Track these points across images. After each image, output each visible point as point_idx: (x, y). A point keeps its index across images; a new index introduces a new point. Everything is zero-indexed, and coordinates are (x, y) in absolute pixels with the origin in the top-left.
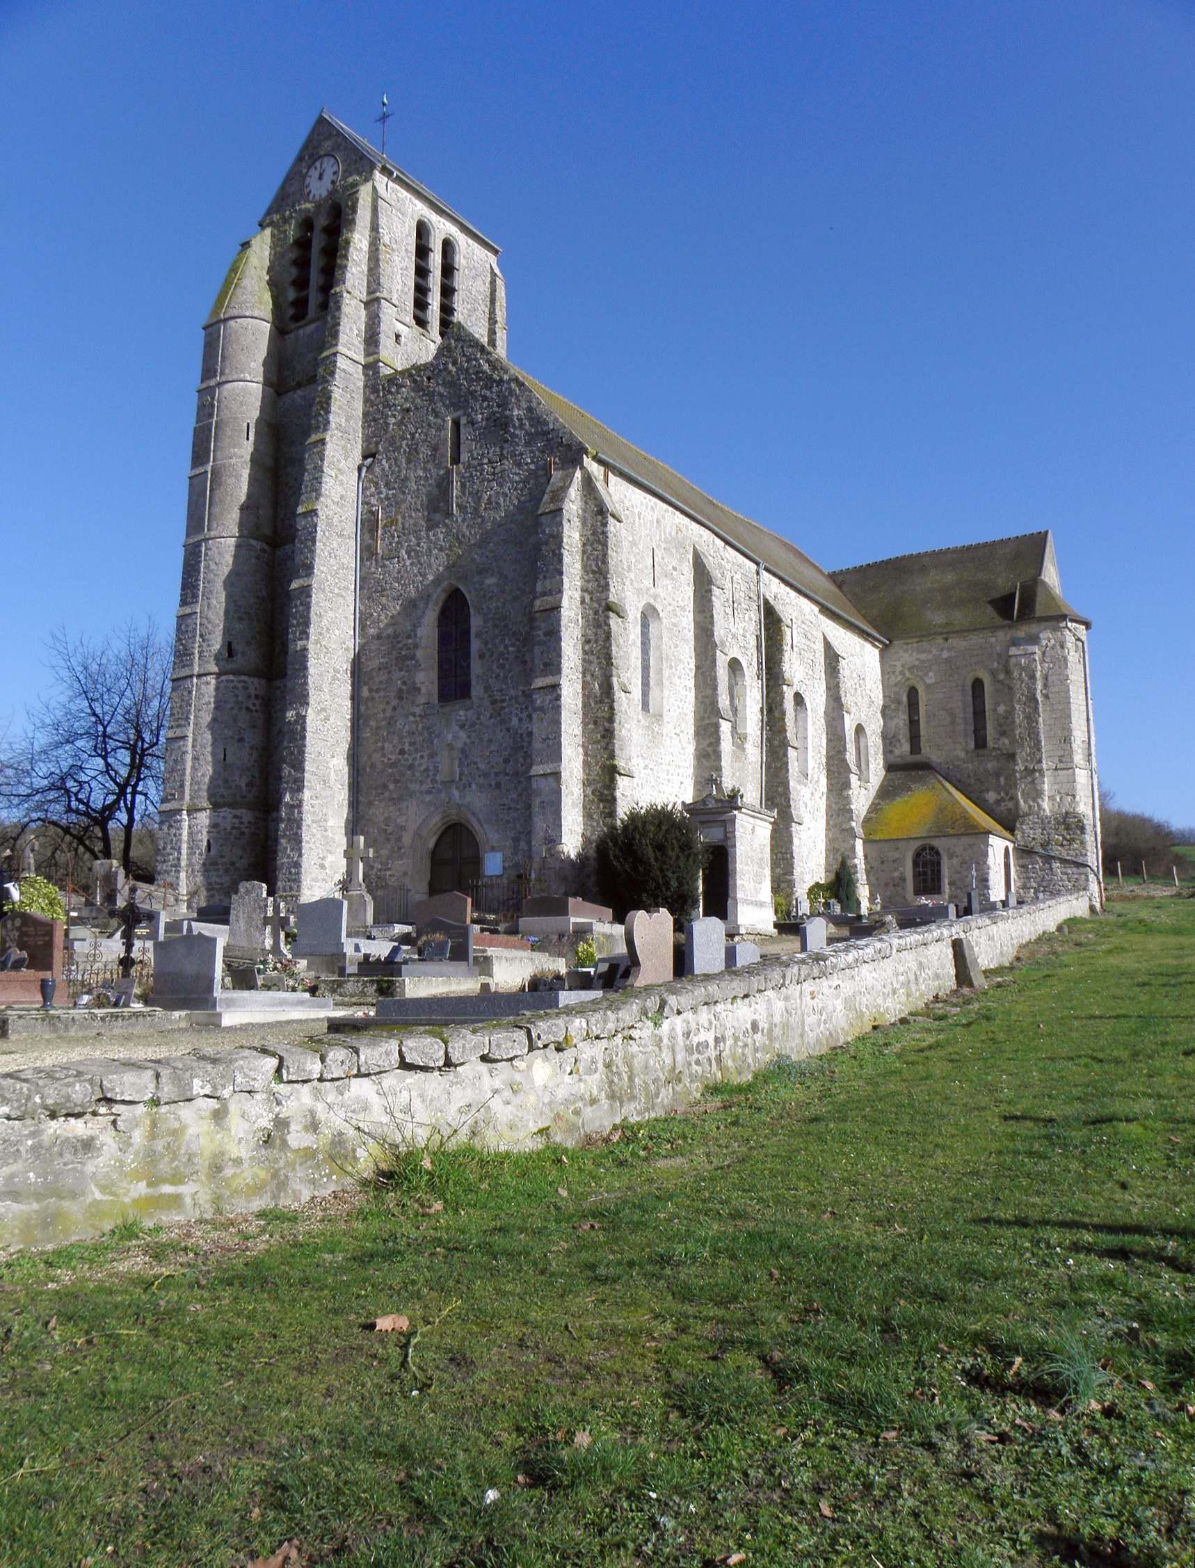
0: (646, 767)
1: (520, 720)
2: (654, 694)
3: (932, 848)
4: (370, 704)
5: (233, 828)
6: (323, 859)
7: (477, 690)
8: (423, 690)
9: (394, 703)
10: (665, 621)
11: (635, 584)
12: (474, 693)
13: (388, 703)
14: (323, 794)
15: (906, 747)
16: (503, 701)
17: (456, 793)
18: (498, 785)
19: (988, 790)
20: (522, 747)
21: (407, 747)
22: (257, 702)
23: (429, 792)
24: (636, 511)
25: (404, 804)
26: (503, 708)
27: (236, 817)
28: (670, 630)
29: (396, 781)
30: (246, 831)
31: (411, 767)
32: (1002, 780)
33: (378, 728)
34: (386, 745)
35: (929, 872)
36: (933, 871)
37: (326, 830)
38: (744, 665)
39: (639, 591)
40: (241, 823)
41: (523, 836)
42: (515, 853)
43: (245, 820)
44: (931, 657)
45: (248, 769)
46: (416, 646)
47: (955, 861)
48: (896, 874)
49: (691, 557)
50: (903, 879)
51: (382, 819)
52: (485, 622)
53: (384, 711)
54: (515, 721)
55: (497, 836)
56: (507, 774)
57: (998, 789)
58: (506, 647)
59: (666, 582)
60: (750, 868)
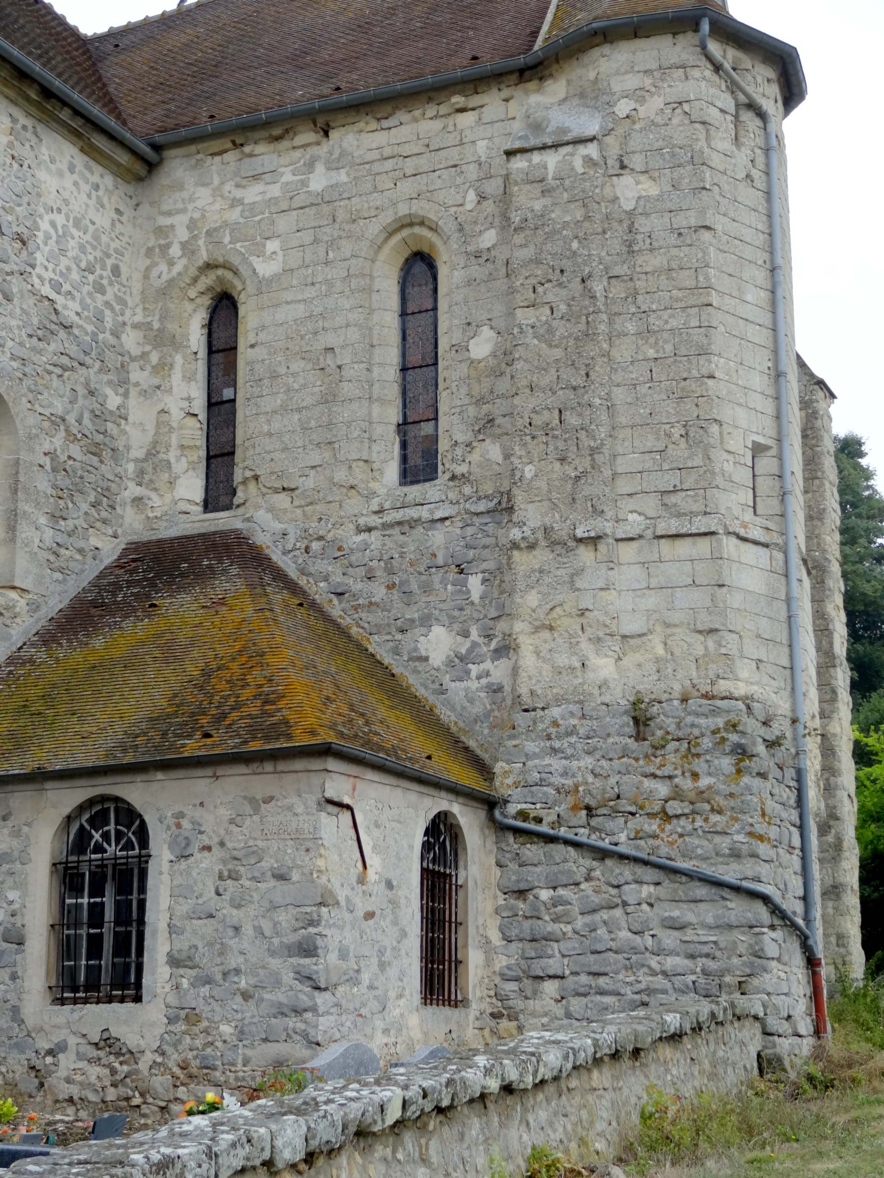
3: (130, 816)
15: (192, 487)
19: (426, 621)
32: (475, 584)
35: (109, 914)
36: (122, 909)
44: (275, 191)
47: (206, 865)
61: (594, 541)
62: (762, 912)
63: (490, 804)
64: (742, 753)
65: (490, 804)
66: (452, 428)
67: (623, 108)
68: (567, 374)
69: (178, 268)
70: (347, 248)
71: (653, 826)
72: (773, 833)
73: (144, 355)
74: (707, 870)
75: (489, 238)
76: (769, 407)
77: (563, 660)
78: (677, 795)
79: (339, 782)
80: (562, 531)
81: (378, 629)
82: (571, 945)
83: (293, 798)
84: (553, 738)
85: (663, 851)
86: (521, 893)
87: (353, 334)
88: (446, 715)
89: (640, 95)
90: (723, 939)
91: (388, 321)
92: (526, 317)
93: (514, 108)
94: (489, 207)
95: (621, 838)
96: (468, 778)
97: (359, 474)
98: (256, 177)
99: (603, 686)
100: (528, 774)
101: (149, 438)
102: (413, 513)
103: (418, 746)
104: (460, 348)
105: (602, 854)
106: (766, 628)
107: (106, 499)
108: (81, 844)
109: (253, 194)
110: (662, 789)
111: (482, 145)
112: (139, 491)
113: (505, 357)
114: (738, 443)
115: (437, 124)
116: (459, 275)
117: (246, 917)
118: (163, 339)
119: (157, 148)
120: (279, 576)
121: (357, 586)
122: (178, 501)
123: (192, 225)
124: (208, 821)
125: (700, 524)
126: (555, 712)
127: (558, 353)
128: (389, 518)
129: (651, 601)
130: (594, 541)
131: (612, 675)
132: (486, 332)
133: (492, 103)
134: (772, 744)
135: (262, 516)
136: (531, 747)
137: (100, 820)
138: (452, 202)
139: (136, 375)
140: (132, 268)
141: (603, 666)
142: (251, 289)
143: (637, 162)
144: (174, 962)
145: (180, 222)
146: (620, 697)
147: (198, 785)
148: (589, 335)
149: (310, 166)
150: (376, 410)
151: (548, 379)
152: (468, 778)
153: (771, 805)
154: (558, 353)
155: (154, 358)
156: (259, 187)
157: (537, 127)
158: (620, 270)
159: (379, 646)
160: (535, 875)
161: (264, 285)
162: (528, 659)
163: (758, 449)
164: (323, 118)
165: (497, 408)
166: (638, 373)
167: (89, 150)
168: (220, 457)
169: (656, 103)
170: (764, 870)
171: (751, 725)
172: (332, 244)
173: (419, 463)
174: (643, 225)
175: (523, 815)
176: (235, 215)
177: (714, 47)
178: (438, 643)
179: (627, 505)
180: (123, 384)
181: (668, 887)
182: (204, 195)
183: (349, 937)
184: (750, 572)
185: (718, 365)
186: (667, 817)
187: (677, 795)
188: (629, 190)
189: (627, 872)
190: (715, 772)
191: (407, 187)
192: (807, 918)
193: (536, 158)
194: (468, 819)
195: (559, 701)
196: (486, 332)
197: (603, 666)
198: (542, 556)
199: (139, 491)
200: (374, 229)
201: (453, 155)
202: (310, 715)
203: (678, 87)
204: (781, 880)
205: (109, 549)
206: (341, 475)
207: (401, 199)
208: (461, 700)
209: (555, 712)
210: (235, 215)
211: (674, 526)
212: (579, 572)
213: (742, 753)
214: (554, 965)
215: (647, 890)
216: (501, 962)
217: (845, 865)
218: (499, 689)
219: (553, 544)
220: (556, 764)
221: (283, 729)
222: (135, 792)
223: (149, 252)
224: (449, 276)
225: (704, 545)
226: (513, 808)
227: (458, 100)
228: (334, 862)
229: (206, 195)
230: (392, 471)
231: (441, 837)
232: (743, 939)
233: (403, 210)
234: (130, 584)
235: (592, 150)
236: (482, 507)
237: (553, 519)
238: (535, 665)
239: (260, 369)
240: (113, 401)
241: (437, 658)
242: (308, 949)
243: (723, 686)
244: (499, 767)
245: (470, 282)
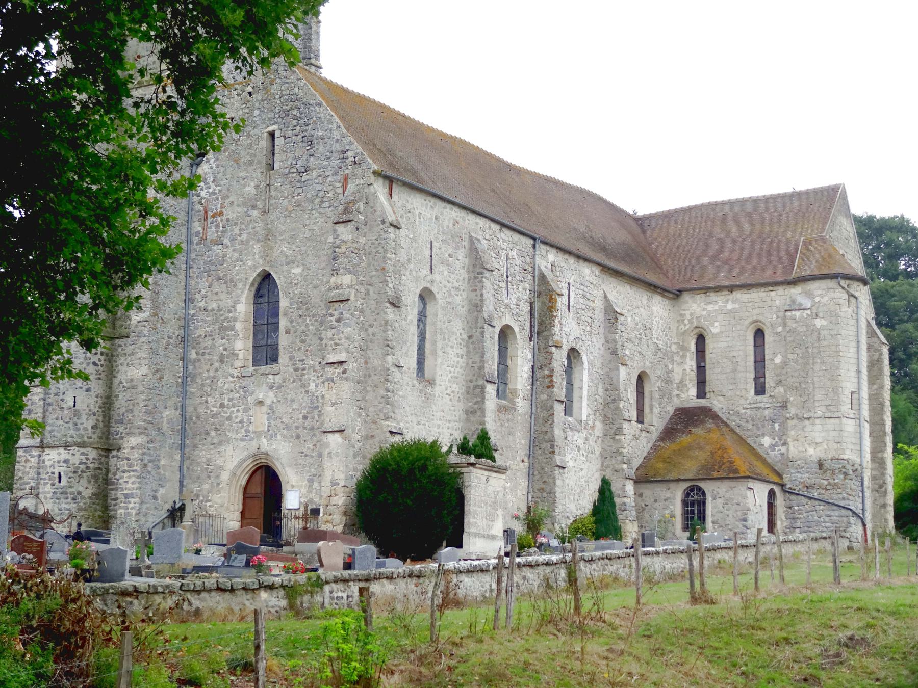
0: (419, 423)
1: (317, 386)
2: (428, 363)
3: (699, 489)
4: (197, 364)
5: (81, 463)
6: (156, 491)
7: (283, 358)
8: (241, 356)
9: (217, 365)
10: (440, 302)
11: (414, 273)
12: (280, 361)
13: (211, 365)
14: (158, 438)
15: (693, 392)
16: (304, 369)
17: (264, 441)
18: (298, 437)
19: (763, 435)
20: (317, 407)
21: (226, 402)
22: (102, 358)
23: (242, 440)
24: (417, 212)
25: (222, 448)
26: (303, 375)
27: (82, 454)
28: (443, 308)
29: (217, 430)
30: (92, 466)
31: (229, 418)
32: (777, 426)
33: (203, 385)
34: (210, 399)
35: (696, 512)
36: (699, 511)
37: (159, 468)
38: (516, 329)
39: (417, 279)
40: (87, 459)
41: (315, 478)
42: (310, 492)
43: (90, 457)
44: (716, 307)
45: (94, 414)
46: (235, 320)
47: (720, 502)
48: (667, 512)
49: (466, 243)
50: (673, 516)
51: (204, 460)
52: (291, 304)
53: (208, 371)
54: (312, 386)
55: (296, 477)
56: (305, 428)
57: (772, 435)
58: (307, 325)
59: (442, 268)
60: (483, 510)
61: (809, 419)
62: (850, 513)
63: (782, 486)
64: (846, 474)
65: (782, 486)
66: (769, 381)
67: (817, 299)
68: (802, 373)
69: (687, 327)
70: (739, 327)
71: (823, 492)
72: (854, 493)
73: (678, 352)
74: (837, 503)
75: (780, 329)
76: (856, 380)
77: (800, 449)
78: (829, 484)
79: (751, 484)
80: (800, 415)
81: (750, 436)
82: (803, 520)
83: (740, 488)
84: (798, 469)
85: (826, 498)
86: (790, 508)
87: (741, 353)
88: (769, 460)
89: (821, 296)
90: (840, 519)
91: (751, 348)
92: (791, 356)
93: (786, 292)
94: (779, 319)
95: (815, 494)
96: (776, 479)
97: (743, 392)
98: (711, 303)
99: (811, 456)
100: (792, 478)
101: (680, 377)
102: (759, 405)
103: (765, 472)
104: (772, 360)
105: (811, 498)
106: (854, 440)
108: (687, 495)
109: (710, 307)
110: (826, 483)
111: (777, 302)
112: (678, 393)
113: (785, 364)
114: (847, 392)
115: (764, 294)
116: (771, 339)
117: (730, 513)
118: (683, 348)
119: (680, 291)
120: (722, 421)
121: (743, 424)
123: (691, 315)
124: (720, 492)
125: (836, 415)
126: (799, 462)
127: (799, 367)
128: (753, 406)
129: (823, 434)
130: (809, 419)
131: (813, 453)
132: (779, 356)
133: (781, 290)
134: (854, 471)
135: (715, 402)
136: (792, 471)
137: (692, 490)
138: (769, 319)
139: (676, 358)
140: (674, 326)
141: (811, 451)
142: (710, 336)
143: (821, 315)
144: (713, 522)
145: (688, 313)
146: (815, 459)
147: (718, 483)
148: (807, 363)
149: (727, 301)
150: (748, 374)
151: (796, 374)
152: (776, 479)
153: (853, 486)
154: (799, 367)
155: (681, 353)
156: (712, 306)
157: (793, 302)
158: (816, 345)
159: (750, 441)
160: (794, 503)
161: (714, 335)
162: (791, 448)
163: (852, 393)
164: (731, 289)
165: (783, 378)
166: (821, 373)
167: (663, 296)
168: (701, 383)
169: (826, 298)
170: (851, 503)
171: (848, 467)
172: (734, 326)
173: (760, 390)
174: (823, 333)
175: (790, 488)
176: (704, 313)
178: (767, 441)
179: (817, 409)
180: (672, 362)
181: (827, 506)
182: (694, 306)
184: (849, 426)
185: (842, 372)
186: (827, 490)
187: (829, 484)
188: (819, 323)
189: (817, 503)
190: (839, 479)
191: (756, 311)
192: (863, 514)
193: (793, 313)
194: (777, 489)
195: (800, 459)
196: (779, 356)
197: (811, 451)
198: (795, 422)
199: (678, 393)
200: (747, 322)
201: (769, 303)
202: (743, 469)
203: (831, 294)
204: (856, 505)
206: (738, 393)
207: (754, 314)
208: (773, 456)
209: (799, 462)
210: (704, 313)
211: (829, 415)
212: (805, 426)
213: (846, 474)
214: (798, 525)
215: (822, 507)
216: (785, 524)
217: (888, 498)
218: (783, 454)
219: (798, 419)
220: (799, 475)
221: (736, 471)
222: (702, 485)
223: (678, 321)
224: (769, 339)
225: (837, 420)
226: (788, 486)
227: (770, 288)
228: (750, 502)
229: (695, 307)
230: (752, 391)
231: (772, 494)
232: (845, 519)
233: (755, 318)
234: (681, 422)
235: (808, 312)
236: (778, 405)
237: (798, 412)
238: (793, 450)
239: (714, 361)
241: (766, 445)
242: (745, 520)
243: (842, 457)
244: (784, 476)
245: (774, 341)
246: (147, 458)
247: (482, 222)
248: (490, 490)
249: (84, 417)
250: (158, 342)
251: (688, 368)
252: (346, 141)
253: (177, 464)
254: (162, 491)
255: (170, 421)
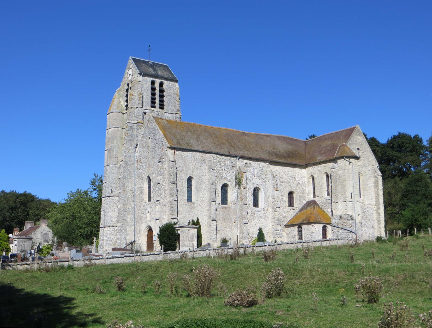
15: (312, 196)
38: (229, 184)
47: (306, 230)
79: (313, 224)
89: (340, 163)
105: (338, 228)
107: (305, 197)
109: (314, 169)
118: (309, 182)
122: (310, 197)
177: (346, 159)
183: (315, 235)
185: (347, 187)
205: (305, 202)
240: (305, 188)
246: (122, 229)
247: (213, 155)
248: (190, 233)
249: (113, 219)
250: (125, 197)
251: (310, 188)
252: (162, 139)
253: (133, 230)
254: (128, 237)
255: (130, 218)
